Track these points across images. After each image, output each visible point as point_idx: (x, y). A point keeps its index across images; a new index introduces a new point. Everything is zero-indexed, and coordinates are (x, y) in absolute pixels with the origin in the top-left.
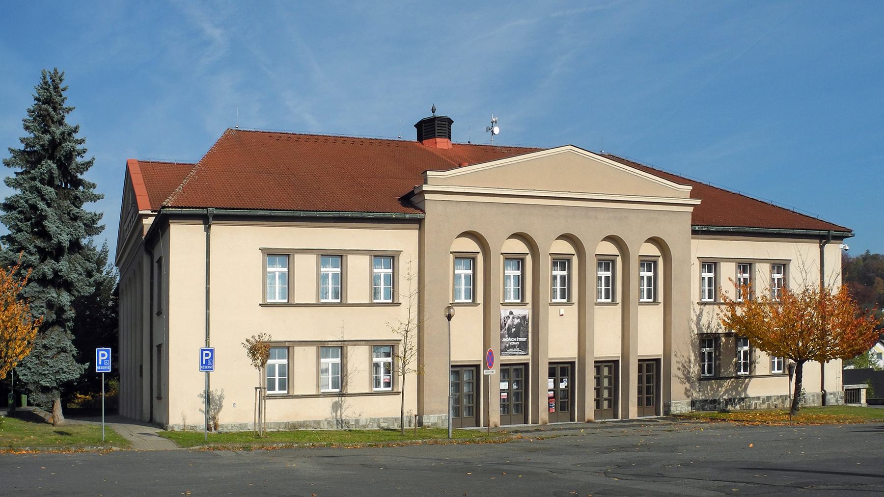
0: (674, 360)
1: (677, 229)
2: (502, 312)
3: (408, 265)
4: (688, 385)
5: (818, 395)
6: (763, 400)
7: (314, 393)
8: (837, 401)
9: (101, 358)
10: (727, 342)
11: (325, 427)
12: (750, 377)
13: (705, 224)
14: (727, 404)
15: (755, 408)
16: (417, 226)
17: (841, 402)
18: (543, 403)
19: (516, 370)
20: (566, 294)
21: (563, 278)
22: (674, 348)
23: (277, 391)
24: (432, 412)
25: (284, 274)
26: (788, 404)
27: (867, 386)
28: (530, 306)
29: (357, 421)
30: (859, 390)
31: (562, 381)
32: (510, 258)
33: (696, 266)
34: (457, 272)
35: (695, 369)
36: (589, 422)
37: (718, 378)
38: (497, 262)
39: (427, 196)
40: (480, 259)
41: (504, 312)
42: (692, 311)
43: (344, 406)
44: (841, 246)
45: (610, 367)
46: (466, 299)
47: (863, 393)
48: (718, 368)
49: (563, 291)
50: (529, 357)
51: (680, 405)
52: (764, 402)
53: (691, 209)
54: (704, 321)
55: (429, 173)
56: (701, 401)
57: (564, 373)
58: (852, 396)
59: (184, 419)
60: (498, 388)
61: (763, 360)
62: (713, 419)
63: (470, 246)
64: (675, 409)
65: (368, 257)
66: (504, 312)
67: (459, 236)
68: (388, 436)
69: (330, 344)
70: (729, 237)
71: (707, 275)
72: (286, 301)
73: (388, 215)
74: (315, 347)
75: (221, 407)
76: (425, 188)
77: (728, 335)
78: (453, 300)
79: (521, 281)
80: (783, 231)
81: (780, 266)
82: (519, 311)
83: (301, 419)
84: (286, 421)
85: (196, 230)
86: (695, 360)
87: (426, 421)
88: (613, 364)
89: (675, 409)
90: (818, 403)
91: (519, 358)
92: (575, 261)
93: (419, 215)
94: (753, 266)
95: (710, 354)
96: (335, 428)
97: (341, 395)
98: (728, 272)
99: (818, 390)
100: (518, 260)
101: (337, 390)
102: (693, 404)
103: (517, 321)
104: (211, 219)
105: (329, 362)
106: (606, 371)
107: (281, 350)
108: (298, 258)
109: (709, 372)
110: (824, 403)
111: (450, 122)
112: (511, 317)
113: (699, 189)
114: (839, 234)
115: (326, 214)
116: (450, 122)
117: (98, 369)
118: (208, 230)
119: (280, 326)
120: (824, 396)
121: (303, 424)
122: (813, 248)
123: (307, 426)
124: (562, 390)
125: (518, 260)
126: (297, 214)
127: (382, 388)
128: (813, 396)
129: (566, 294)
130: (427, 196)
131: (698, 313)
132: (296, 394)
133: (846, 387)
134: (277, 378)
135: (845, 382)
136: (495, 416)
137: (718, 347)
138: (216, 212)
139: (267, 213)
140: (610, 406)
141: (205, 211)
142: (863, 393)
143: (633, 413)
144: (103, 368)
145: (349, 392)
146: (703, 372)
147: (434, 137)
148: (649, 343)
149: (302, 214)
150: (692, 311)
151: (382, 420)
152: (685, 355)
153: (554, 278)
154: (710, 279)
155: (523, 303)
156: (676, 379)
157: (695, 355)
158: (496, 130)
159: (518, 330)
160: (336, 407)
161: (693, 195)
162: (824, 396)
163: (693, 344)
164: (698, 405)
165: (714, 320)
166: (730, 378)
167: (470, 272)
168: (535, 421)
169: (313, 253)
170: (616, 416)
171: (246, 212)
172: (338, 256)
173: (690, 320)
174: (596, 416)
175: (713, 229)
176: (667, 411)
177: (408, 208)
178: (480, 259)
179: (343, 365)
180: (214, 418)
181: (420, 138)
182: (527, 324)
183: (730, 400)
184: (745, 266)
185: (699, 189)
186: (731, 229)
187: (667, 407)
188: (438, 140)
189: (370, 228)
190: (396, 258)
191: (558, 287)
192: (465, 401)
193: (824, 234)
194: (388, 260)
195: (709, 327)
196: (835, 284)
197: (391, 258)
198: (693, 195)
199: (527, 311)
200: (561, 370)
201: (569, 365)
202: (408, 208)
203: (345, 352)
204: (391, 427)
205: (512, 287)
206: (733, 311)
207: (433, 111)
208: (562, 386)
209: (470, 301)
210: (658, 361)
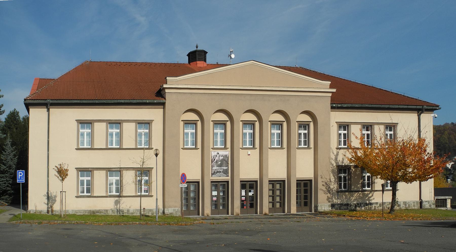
0: (320, 180)
1: (322, 107)
2: (212, 153)
3: (157, 128)
4: (329, 195)
5: (417, 202)
6: (380, 204)
7: (134, 195)
8: (430, 206)
9: (19, 176)
10: (356, 171)
11: (110, 213)
12: (371, 191)
13: (338, 104)
14: (356, 207)
15: (375, 209)
16: (162, 107)
17: (433, 207)
18: (237, 204)
19: (221, 185)
20: (307, 142)
21: (305, 134)
22: (320, 173)
23: (85, 194)
24: (170, 207)
26: (390, 206)
27: (451, 197)
28: (229, 150)
30: (446, 200)
31: (250, 191)
32: (246, 123)
33: (335, 127)
34: (186, 131)
35: (334, 186)
36: (266, 214)
37: (351, 191)
38: (267, 126)
40: (285, 124)
41: (214, 153)
42: (331, 153)
43: (121, 202)
44: (433, 115)
45: (280, 184)
47: (449, 202)
48: (350, 186)
49: (305, 142)
50: (229, 178)
51: (324, 206)
52: (380, 206)
54: (340, 158)
55: (167, 78)
56: (338, 204)
57: (251, 187)
58: (441, 203)
59: (36, 207)
60: (209, 195)
61: (379, 182)
62: (339, 215)
63: (193, 117)
64: (320, 209)
67: (301, 114)
68: (144, 218)
69: (113, 170)
70: (356, 110)
71: (342, 132)
72: (119, 147)
73: (144, 101)
74: (134, 171)
76: (165, 86)
77: (356, 167)
78: (184, 146)
79: (281, 136)
80: (391, 106)
81: (391, 127)
82: (222, 153)
83: (98, 208)
85: (43, 111)
86: (335, 181)
87: (166, 212)
88: (282, 182)
89: (320, 209)
90: (417, 207)
91: (223, 178)
92: (312, 125)
93: (162, 101)
94: (373, 127)
95: (345, 177)
96: (116, 214)
97: (119, 196)
98: (356, 130)
99: (418, 199)
100: (279, 125)
101: (118, 194)
102: (333, 206)
103: (221, 158)
104: (49, 105)
105: (114, 179)
106: (278, 186)
107: (88, 172)
108: (96, 124)
109: (345, 187)
110: (421, 207)
111: (205, 53)
112: (218, 155)
113: (335, 82)
114: (431, 108)
115: (110, 101)
116: (205, 53)
117: (18, 181)
118: (48, 110)
120: (421, 203)
121: (99, 211)
122: (413, 117)
123: (101, 212)
124: (250, 196)
125: (279, 125)
126: (95, 101)
128: (414, 202)
129: (307, 142)
130: (167, 91)
131: (335, 154)
132: (95, 195)
133: (436, 198)
134: (85, 187)
135: (436, 194)
136: (208, 210)
137: (350, 174)
138: (51, 102)
139: (78, 101)
140: (280, 206)
141: (46, 102)
142: (449, 202)
143: (294, 210)
144: (20, 180)
145: (124, 195)
146: (340, 187)
147: (196, 61)
148: (304, 169)
149: (97, 102)
150: (331, 153)
152: (328, 178)
153: (300, 134)
154: (391, 135)
155: (225, 148)
156: (321, 191)
157: (335, 178)
158: (233, 56)
159: (224, 162)
160: (117, 203)
161: (331, 87)
162: (421, 203)
163: (333, 171)
164: (336, 206)
165: (345, 157)
166: (359, 191)
167: (252, 131)
168: (232, 213)
169: (104, 122)
170: (284, 211)
171: (68, 101)
172: (118, 123)
173: (330, 158)
174: (270, 212)
175: (345, 106)
176: (316, 209)
177: (158, 98)
178: (285, 124)
179: (121, 181)
180: (51, 207)
181: (190, 62)
182: (228, 160)
183: (358, 204)
184: (368, 127)
185: (335, 82)
186: (357, 106)
187: (316, 207)
188: (198, 62)
189: (355, 112)
190: (150, 124)
191: (342, 140)
192: (192, 201)
193: (420, 107)
194: (278, 126)
195: (343, 162)
196: (429, 136)
197: (148, 123)
198: (331, 87)
199: (227, 153)
200: (248, 185)
201: (309, 182)
202: (158, 98)
203: (121, 174)
204: (147, 214)
205: (276, 139)
206: (356, 153)
207: (197, 47)
208: (250, 194)
209: (252, 147)
210: (311, 181)
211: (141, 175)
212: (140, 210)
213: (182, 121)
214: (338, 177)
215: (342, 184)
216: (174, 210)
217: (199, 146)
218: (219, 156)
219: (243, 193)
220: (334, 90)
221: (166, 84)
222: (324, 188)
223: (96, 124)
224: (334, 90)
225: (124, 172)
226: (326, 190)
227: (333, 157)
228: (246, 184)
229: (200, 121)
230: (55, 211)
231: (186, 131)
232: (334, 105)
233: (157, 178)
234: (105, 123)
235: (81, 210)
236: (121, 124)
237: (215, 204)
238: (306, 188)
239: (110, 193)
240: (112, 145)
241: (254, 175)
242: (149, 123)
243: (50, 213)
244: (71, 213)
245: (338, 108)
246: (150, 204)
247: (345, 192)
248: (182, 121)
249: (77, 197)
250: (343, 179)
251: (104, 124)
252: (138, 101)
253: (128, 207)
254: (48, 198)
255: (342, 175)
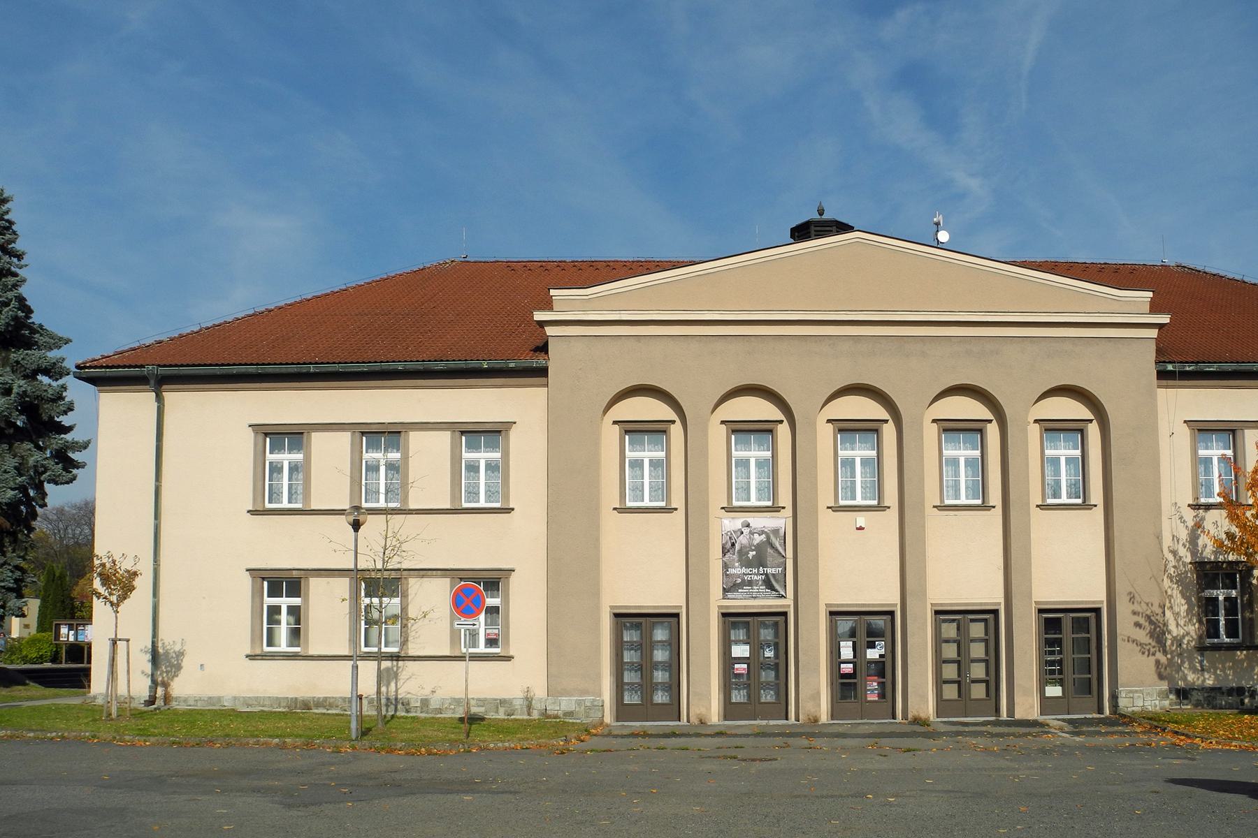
0: (1124, 610)
1: (1125, 371)
3: (528, 450)
4: (1159, 656)
13: (1178, 366)
25: (975, 459)
28: (788, 512)
29: (529, 703)
31: (872, 645)
39: (550, 331)
41: (732, 523)
43: (403, 676)
46: (1069, 497)
50: (789, 601)
53: (1154, 333)
56: (1203, 689)
57: (873, 636)
65: (448, 433)
66: (732, 523)
70: (1178, 382)
74: (448, 580)
75: (179, 667)
78: (1044, 498)
82: (761, 522)
84: (291, 695)
86: (1189, 611)
103: (758, 539)
106: (977, 630)
108: (317, 438)
112: (746, 531)
113: (1174, 287)
118: (159, 399)
119: (288, 546)
126: (304, 369)
127: (482, 648)
131: (1191, 523)
132: (311, 652)
140: (882, 695)
145: (412, 653)
146: (1212, 630)
151: (473, 703)
155: (775, 509)
159: (761, 555)
161: (1155, 308)
164: (1196, 696)
169: (344, 430)
172: (387, 435)
175: (1213, 368)
180: (165, 685)
187: (1114, 697)
197: (492, 433)
198: (1155, 308)
199: (781, 522)
200: (869, 625)
208: (873, 654)
211: (275, 591)
212: (379, 699)
213: (1036, 421)
214: (1199, 599)
215: (1222, 623)
216: (579, 703)
217: (995, 497)
218: (752, 533)
219: (847, 651)
220: (1165, 319)
221: (551, 309)
222: (1142, 636)
223: (317, 438)
224: (1165, 319)
225: (412, 581)
226: (1147, 640)
227: (1184, 535)
228: (1059, 619)
229: (891, 422)
230: (177, 699)
231: (1049, 452)
232: (1170, 367)
233: (526, 605)
234: (348, 434)
235: (264, 698)
236: (1238, 433)
237: (845, 686)
238: (1073, 638)
239: (270, 644)
240: (957, 497)
241: (879, 591)
242: (1233, 431)
243: (159, 703)
244: (228, 704)
245: (1185, 375)
246: (487, 685)
247: (1232, 648)
248: (1036, 421)
249: (251, 657)
250: (1221, 607)
251: (345, 438)
252: (452, 365)
253: (426, 692)
254: (155, 658)
255: (1221, 595)
